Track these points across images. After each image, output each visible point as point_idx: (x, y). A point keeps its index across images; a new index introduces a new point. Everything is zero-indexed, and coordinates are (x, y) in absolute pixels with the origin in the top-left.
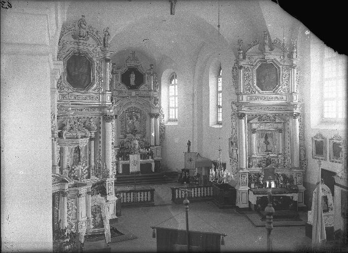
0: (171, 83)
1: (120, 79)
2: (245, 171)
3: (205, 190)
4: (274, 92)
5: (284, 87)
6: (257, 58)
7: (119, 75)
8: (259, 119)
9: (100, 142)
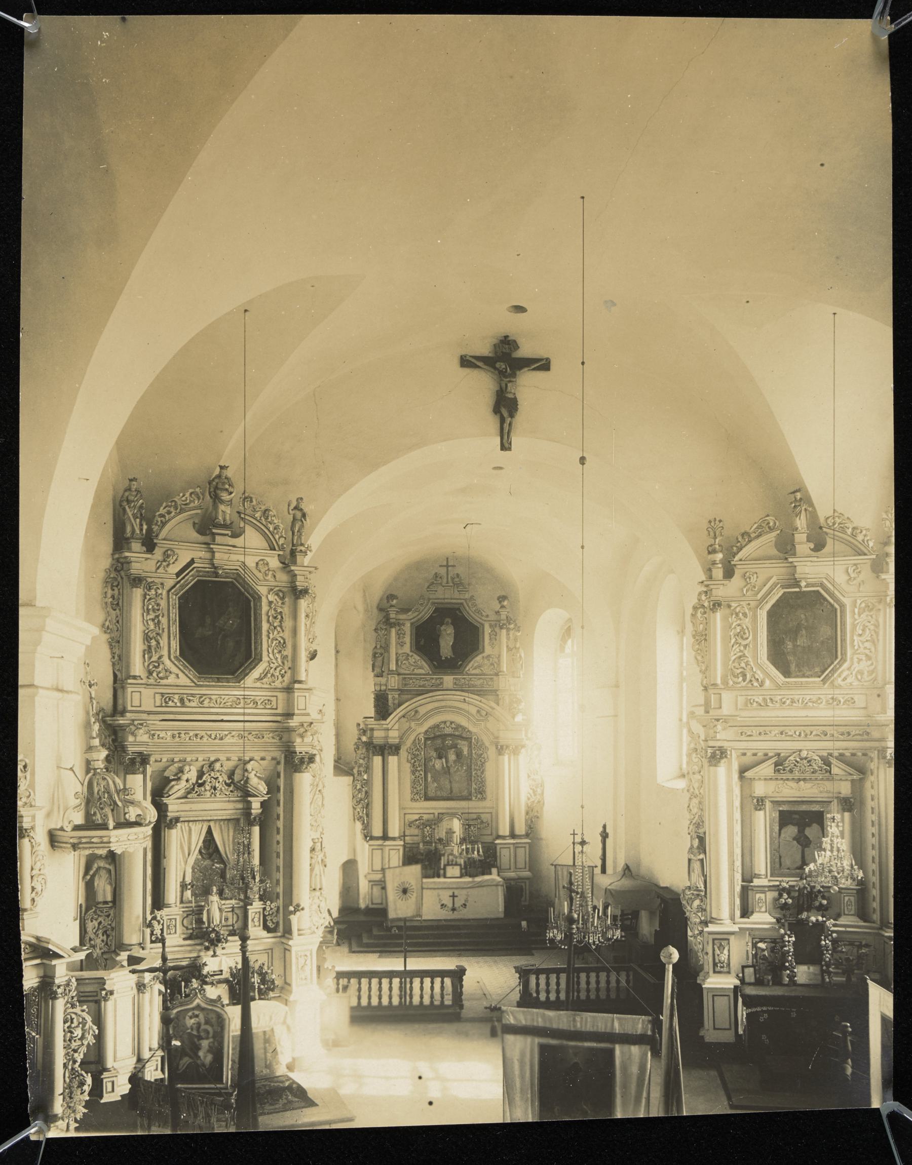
0: (562, 649)
1: (407, 639)
2: (727, 926)
3: (593, 979)
4: (824, 681)
5: (857, 667)
6: (774, 572)
7: (407, 628)
8: (776, 764)
9: (278, 829)
